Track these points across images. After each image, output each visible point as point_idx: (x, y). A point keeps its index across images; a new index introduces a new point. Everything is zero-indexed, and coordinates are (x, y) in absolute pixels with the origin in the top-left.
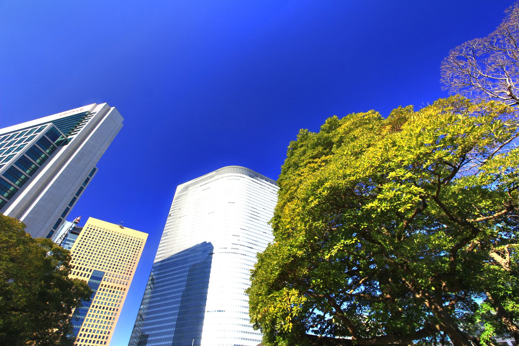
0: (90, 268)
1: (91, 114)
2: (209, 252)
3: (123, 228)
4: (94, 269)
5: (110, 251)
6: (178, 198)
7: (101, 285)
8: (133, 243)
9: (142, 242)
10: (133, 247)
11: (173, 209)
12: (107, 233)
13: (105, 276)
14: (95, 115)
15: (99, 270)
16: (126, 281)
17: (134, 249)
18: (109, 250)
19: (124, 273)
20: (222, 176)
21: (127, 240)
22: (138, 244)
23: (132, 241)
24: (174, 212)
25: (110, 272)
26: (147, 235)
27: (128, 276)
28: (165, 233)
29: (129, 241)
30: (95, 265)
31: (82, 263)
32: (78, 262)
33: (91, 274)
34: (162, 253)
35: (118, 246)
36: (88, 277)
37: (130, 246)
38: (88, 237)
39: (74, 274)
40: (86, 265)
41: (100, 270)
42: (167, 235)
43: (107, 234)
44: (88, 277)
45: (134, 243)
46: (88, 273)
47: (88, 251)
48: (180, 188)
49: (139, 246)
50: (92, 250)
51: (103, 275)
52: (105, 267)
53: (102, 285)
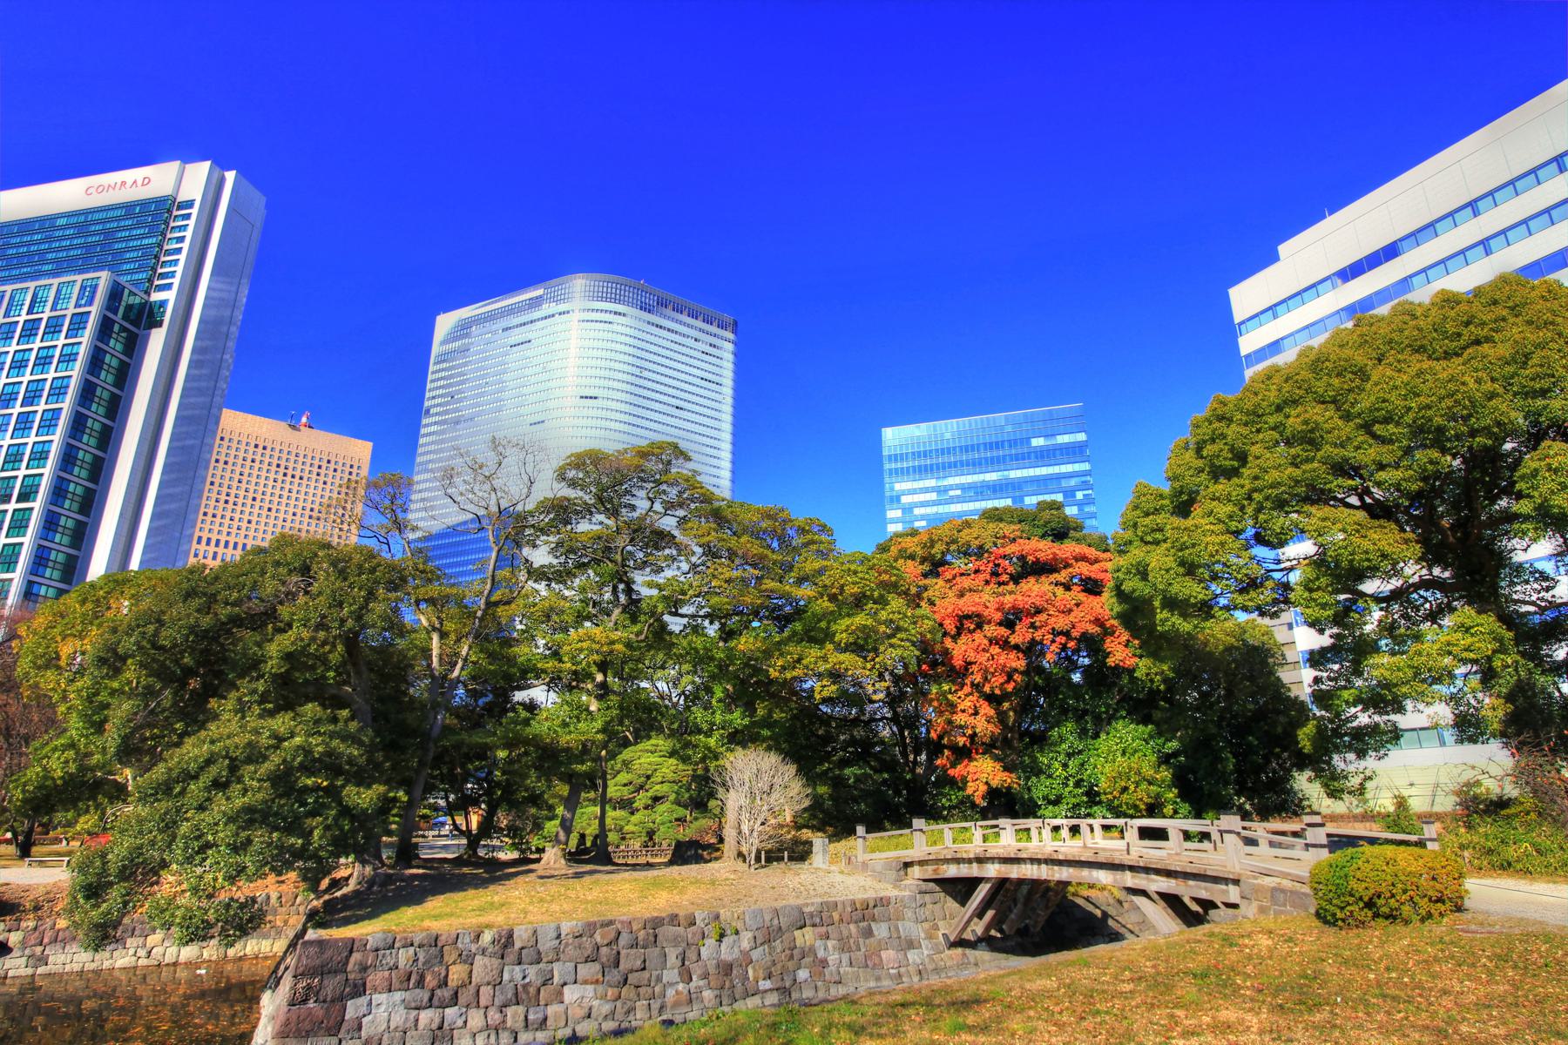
14: (195, 211)
20: (562, 307)
21: (316, 462)
23: (332, 466)
26: (370, 445)
28: (421, 464)
47: (223, 497)
48: (445, 323)
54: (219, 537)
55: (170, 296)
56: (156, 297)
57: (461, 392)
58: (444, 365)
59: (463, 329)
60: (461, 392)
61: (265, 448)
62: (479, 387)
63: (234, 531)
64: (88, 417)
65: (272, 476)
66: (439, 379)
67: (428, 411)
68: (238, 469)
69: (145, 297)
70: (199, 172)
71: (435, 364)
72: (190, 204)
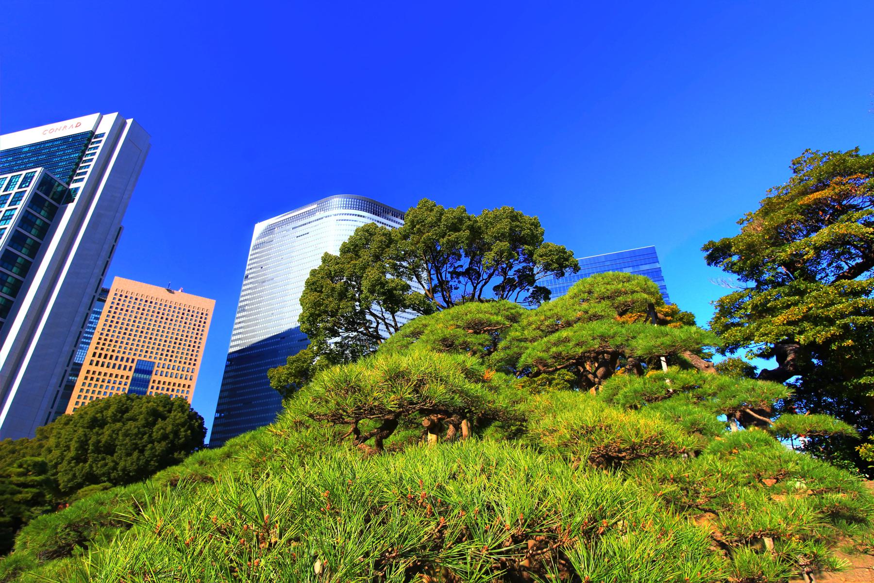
0: (131, 357)
1: (97, 137)
2: (226, 394)
3: (173, 293)
4: (137, 358)
5: (158, 331)
6: (257, 247)
7: (152, 381)
8: (192, 316)
9: (207, 314)
10: (193, 322)
11: (251, 266)
12: (149, 302)
13: (156, 368)
14: (104, 139)
15: (145, 359)
16: (190, 374)
17: (189, 346)
18: (156, 328)
19: (185, 363)
20: (327, 213)
21: (182, 311)
22: (192, 355)
23: (191, 313)
24: (252, 271)
25: (162, 362)
26: (214, 301)
27: (191, 367)
28: (241, 307)
29: (186, 313)
30: (138, 353)
31: (117, 349)
32: (111, 348)
33: (134, 365)
34: (239, 339)
35: (169, 321)
36: (130, 370)
37: (188, 322)
38: (119, 309)
39: (108, 367)
40: (124, 353)
41: (147, 359)
42: (244, 310)
43: (148, 304)
44: (130, 370)
45: (189, 337)
46: (129, 364)
47: (123, 331)
48: (259, 228)
49: (194, 358)
50: (129, 330)
51: (153, 366)
52: (154, 355)
53: (154, 381)
54: (118, 355)
55: (81, 185)
56: (73, 186)
57: (266, 264)
58: (257, 251)
59: (270, 230)
60: (266, 264)
61: (151, 302)
62: (268, 316)
63: (128, 351)
64: (19, 256)
65: (154, 319)
66: (254, 259)
67: (247, 277)
68: (134, 315)
69: (67, 186)
70: (109, 121)
71: (253, 250)
72: (102, 135)
